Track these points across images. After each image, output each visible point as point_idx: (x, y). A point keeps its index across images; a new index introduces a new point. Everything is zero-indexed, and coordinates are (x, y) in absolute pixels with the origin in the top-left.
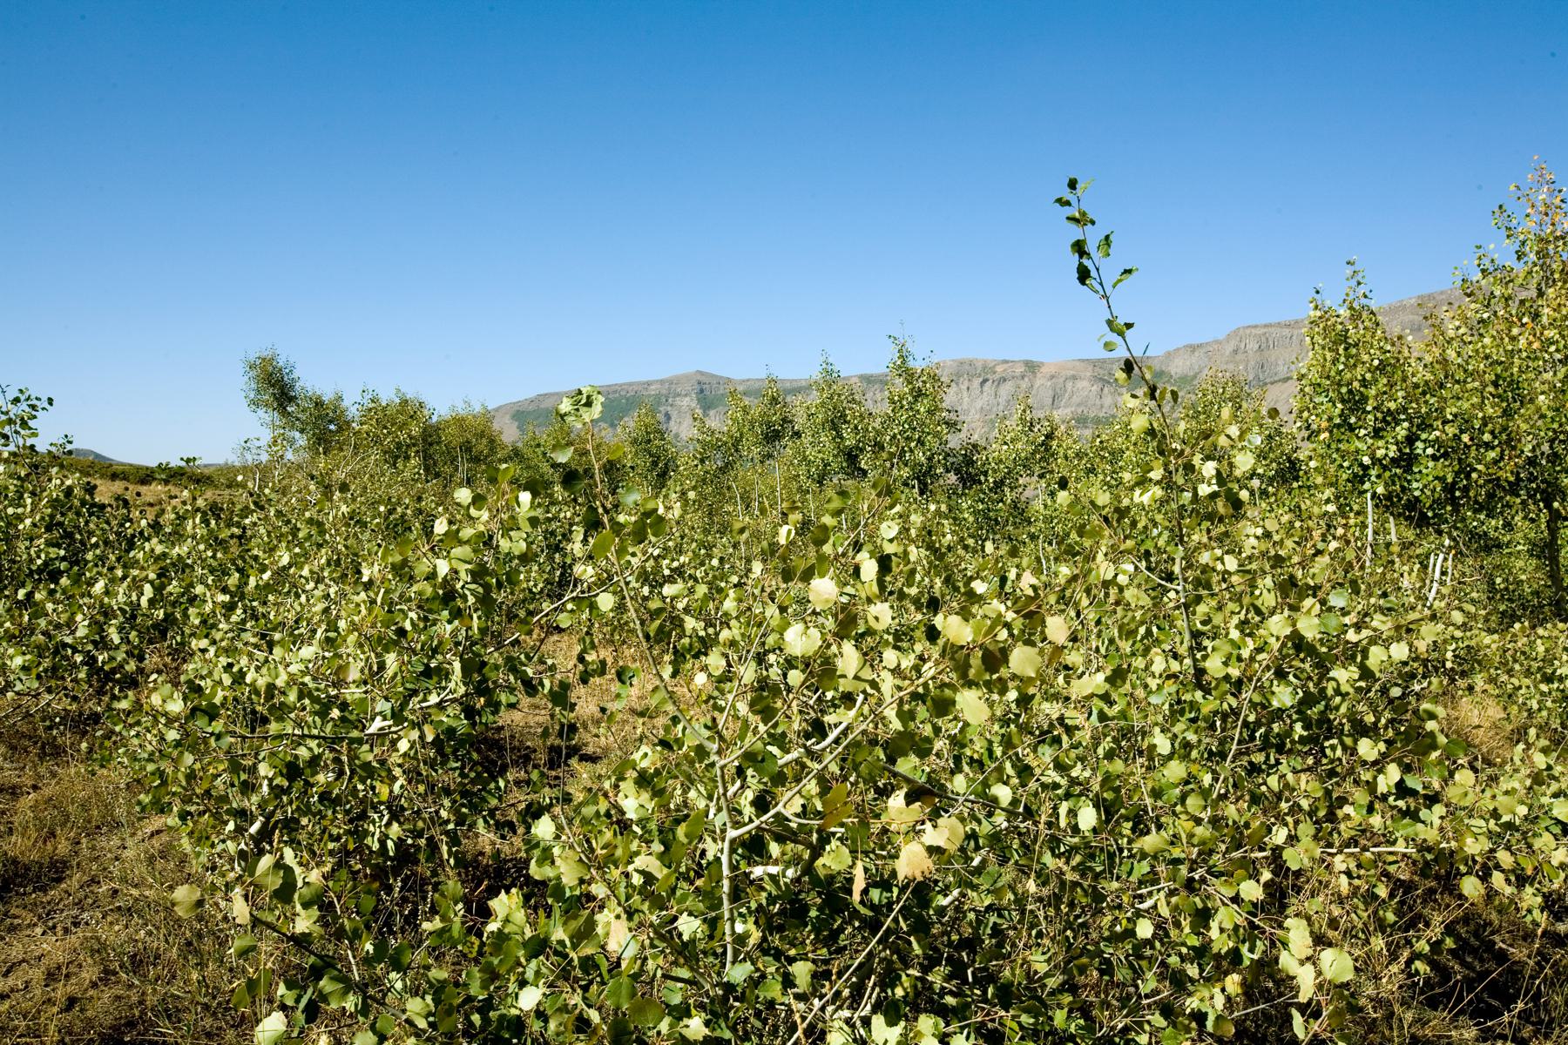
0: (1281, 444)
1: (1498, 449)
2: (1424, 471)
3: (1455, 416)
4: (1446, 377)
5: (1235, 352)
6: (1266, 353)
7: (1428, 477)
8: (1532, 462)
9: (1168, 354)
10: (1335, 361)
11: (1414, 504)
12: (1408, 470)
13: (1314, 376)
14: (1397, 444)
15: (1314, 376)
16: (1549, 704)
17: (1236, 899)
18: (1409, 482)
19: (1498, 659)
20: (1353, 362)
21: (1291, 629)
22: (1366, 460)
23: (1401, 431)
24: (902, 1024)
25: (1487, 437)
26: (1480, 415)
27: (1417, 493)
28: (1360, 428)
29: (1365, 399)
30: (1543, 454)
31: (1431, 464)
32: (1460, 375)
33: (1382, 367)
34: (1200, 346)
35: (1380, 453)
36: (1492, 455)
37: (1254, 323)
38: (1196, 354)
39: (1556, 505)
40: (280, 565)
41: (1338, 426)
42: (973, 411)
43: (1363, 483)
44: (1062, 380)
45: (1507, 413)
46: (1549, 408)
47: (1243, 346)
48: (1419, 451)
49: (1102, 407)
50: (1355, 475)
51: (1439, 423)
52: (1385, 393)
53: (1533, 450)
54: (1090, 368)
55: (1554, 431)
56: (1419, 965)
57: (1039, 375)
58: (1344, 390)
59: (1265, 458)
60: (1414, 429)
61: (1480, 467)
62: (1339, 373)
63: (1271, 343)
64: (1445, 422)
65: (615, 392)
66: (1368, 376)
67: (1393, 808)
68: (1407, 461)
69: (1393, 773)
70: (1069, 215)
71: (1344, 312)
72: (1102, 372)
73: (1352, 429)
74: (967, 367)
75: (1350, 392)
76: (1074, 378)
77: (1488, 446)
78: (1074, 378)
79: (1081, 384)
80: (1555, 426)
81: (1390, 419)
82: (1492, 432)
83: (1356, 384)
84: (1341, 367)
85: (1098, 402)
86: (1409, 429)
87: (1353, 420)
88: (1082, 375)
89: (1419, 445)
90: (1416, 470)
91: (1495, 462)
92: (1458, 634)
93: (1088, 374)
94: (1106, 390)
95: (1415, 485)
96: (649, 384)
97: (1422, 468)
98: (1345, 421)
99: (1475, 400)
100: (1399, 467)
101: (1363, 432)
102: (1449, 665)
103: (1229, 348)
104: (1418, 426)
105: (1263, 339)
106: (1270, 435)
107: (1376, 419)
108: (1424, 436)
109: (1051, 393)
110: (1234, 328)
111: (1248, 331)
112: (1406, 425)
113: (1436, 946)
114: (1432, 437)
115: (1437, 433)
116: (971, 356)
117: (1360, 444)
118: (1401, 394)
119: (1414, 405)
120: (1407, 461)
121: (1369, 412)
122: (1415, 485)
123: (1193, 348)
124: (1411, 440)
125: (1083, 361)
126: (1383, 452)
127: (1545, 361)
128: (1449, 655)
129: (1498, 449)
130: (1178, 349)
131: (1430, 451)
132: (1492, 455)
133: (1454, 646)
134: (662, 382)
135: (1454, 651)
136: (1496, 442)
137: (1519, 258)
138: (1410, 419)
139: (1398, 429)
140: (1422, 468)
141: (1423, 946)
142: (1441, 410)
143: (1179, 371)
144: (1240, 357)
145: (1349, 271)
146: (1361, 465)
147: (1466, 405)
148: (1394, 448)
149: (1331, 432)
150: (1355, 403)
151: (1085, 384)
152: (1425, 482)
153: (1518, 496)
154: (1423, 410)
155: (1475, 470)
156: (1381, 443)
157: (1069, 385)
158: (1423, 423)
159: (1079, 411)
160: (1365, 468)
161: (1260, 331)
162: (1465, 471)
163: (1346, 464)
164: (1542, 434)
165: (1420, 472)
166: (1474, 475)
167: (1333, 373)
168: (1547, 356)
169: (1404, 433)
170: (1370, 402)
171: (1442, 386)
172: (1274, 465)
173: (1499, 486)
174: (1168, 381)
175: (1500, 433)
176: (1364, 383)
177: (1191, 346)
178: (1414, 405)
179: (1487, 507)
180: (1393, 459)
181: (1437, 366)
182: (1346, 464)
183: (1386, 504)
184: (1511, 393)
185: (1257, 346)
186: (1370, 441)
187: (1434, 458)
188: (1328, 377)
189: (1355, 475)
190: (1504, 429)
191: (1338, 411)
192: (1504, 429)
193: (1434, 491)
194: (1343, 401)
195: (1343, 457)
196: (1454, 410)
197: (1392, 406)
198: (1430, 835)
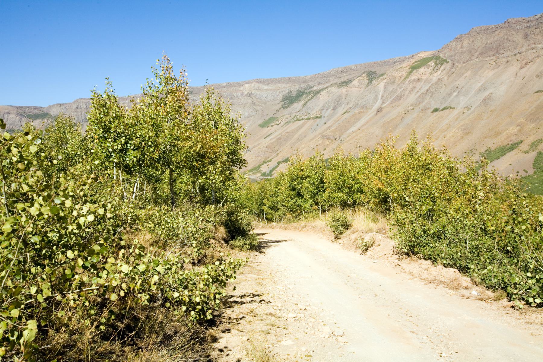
0: (87, 144)
1: (153, 148)
2: (131, 154)
3: (140, 136)
4: (137, 122)
5: (77, 108)
7: (132, 157)
8: (164, 152)
9: (50, 107)
10: (100, 114)
11: (127, 166)
12: (125, 154)
13: (93, 119)
14: (121, 145)
15: (93, 119)
16: (164, 232)
18: (126, 158)
19: (144, 218)
20: (107, 114)
21: (39, 212)
22: (111, 150)
23: (123, 140)
25: (150, 143)
26: (148, 136)
27: (128, 162)
28: (109, 138)
29: (110, 128)
30: (167, 150)
31: (132, 152)
32: (142, 122)
33: (116, 117)
34: (63, 104)
35: (115, 148)
36: (151, 149)
38: (61, 107)
39: (171, 166)
41: (101, 137)
43: (110, 158)
44: (2, 114)
45: (157, 136)
46: (168, 135)
48: (129, 147)
50: (107, 155)
51: (135, 138)
52: (117, 126)
53: (164, 148)
54: (16, 110)
55: (170, 142)
56: (102, 327)
58: (103, 124)
59: (80, 149)
60: (127, 140)
61: (148, 154)
62: (101, 118)
64: (137, 138)
66: (112, 120)
67: (92, 273)
68: (124, 151)
69: (80, 262)
71: (105, 96)
72: (21, 111)
73: (106, 139)
75: (105, 125)
76: (8, 113)
77: (150, 146)
78: (8, 113)
79: (11, 116)
80: (170, 140)
81: (119, 135)
82: (151, 142)
83: (107, 123)
84: (102, 116)
85: (19, 124)
86: (125, 140)
87: (106, 135)
88: (12, 112)
89: (129, 145)
90: (128, 154)
91: (153, 152)
92: (132, 211)
93: (15, 112)
94: (23, 119)
95: (127, 159)
97: (130, 153)
98: (103, 136)
99: (146, 131)
100: (122, 153)
101: (110, 140)
102: (129, 221)
103: (74, 106)
104: (128, 139)
106: (82, 140)
107: (114, 136)
108: (130, 142)
110: (76, 99)
111: (82, 100)
112: (124, 138)
113: (108, 320)
114: (132, 143)
115: (134, 141)
117: (109, 144)
118: (122, 127)
119: (126, 131)
120: (124, 151)
121: (112, 133)
122: (127, 159)
123: (60, 105)
124: (126, 143)
125: (12, 106)
126: (116, 147)
127: (168, 119)
128: (129, 218)
129: (153, 148)
130: (54, 105)
131: (132, 147)
132: (151, 149)
133: (131, 215)
135: (131, 217)
136: (153, 145)
137: (160, 85)
138: (126, 136)
139: (122, 139)
140: (130, 153)
141: (103, 320)
142: (135, 134)
143: (55, 114)
144: (78, 110)
145: (106, 82)
146: (109, 152)
147: (143, 132)
148: (120, 146)
149: (99, 139)
150: (107, 130)
151: (13, 116)
152: (130, 158)
153: (159, 163)
154: (130, 133)
155: (146, 154)
156: (115, 144)
158: (130, 138)
159: (11, 127)
160: (111, 153)
161: (87, 101)
162: (143, 154)
163: (104, 151)
164: (167, 143)
165: (129, 155)
166: (146, 156)
167: (99, 118)
168: (168, 117)
169: (123, 141)
170: (112, 129)
171: (136, 125)
172: (84, 151)
173: (154, 160)
174: (50, 117)
175: (154, 142)
176: (110, 122)
177: (59, 104)
178: (126, 131)
179: (152, 166)
180: (120, 150)
181: (135, 118)
182: (104, 151)
183: (118, 165)
184: (157, 128)
185: (85, 106)
186: (112, 143)
187: (134, 150)
188: (97, 119)
189: (107, 155)
190: (155, 141)
191: (101, 132)
192: (155, 141)
193: (133, 162)
194: (103, 128)
195: (103, 149)
196: (140, 134)
197: (119, 131)
198: (101, 281)
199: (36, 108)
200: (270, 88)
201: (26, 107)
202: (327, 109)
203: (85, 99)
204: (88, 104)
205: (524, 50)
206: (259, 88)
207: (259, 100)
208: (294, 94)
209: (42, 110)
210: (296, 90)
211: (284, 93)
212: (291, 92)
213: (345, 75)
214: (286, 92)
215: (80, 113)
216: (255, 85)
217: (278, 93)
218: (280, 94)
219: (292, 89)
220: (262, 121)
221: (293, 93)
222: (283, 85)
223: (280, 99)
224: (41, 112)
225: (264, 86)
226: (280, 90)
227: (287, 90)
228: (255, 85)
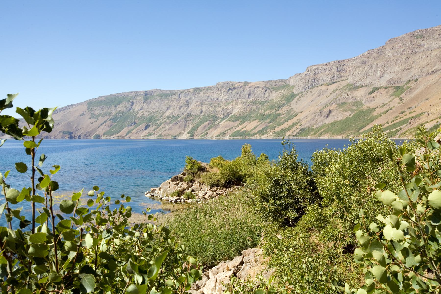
6: (317, 76)
17: (304, 198)
24: (184, 269)
37: (314, 64)
38: (298, 77)
40: (216, 115)
42: (223, 100)
44: (253, 88)
47: (309, 73)
49: (264, 97)
57: (247, 87)
63: (319, 71)
65: (121, 95)
70: (408, 107)
74: (226, 84)
76: (258, 87)
85: (263, 96)
96: (132, 92)
105: (317, 70)
109: (248, 93)
111: (312, 67)
116: (229, 81)
125: (263, 81)
134: (134, 92)
157: (256, 90)
185: (314, 73)
201: (274, 81)
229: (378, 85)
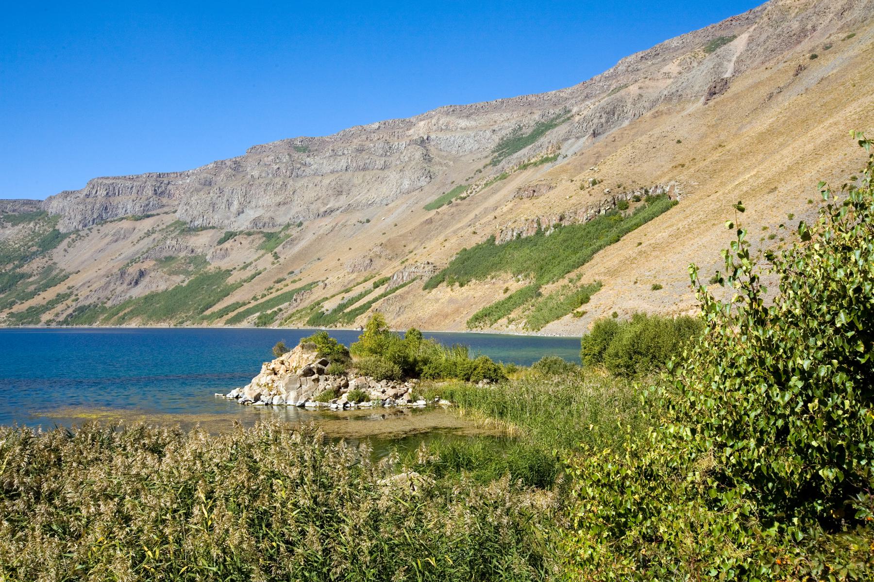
111: (100, 181)
161: (111, 181)
185: (105, 193)
199: (28, 202)
200: (473, 123)
201: (9, 201)
202: (578, 138)
203: (107, 178)
204: (111, 188)
205: (620, 499)
206: (447, 126)
207: (444, 154)
208: (527, 132)
209: (38, 206)
210: (532, 123)
211: (504, 132)
212: (520, 128)
213: (650, 63)
214: (507, 131)
215: (90, 207)
216: (438, 119)
217: (488, 133)
218: (494, 137)
219: (525, 121)
220: (436, 198)
221: (524, 130)
222: (505, 115)
223: (492, 146)
224: (35, 210)
225: (460, 121)
226: (496, 127)
227: (512, 125)
228: (438, 119)
229: (234, 228)
